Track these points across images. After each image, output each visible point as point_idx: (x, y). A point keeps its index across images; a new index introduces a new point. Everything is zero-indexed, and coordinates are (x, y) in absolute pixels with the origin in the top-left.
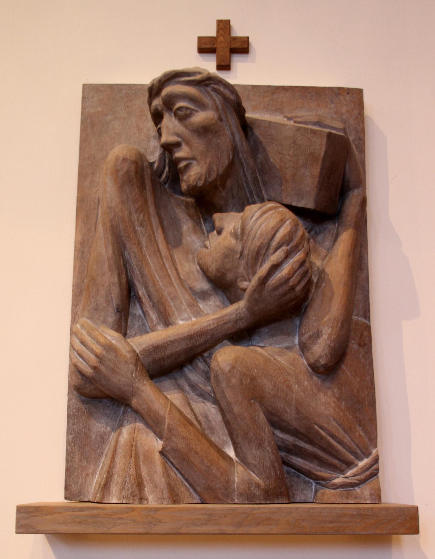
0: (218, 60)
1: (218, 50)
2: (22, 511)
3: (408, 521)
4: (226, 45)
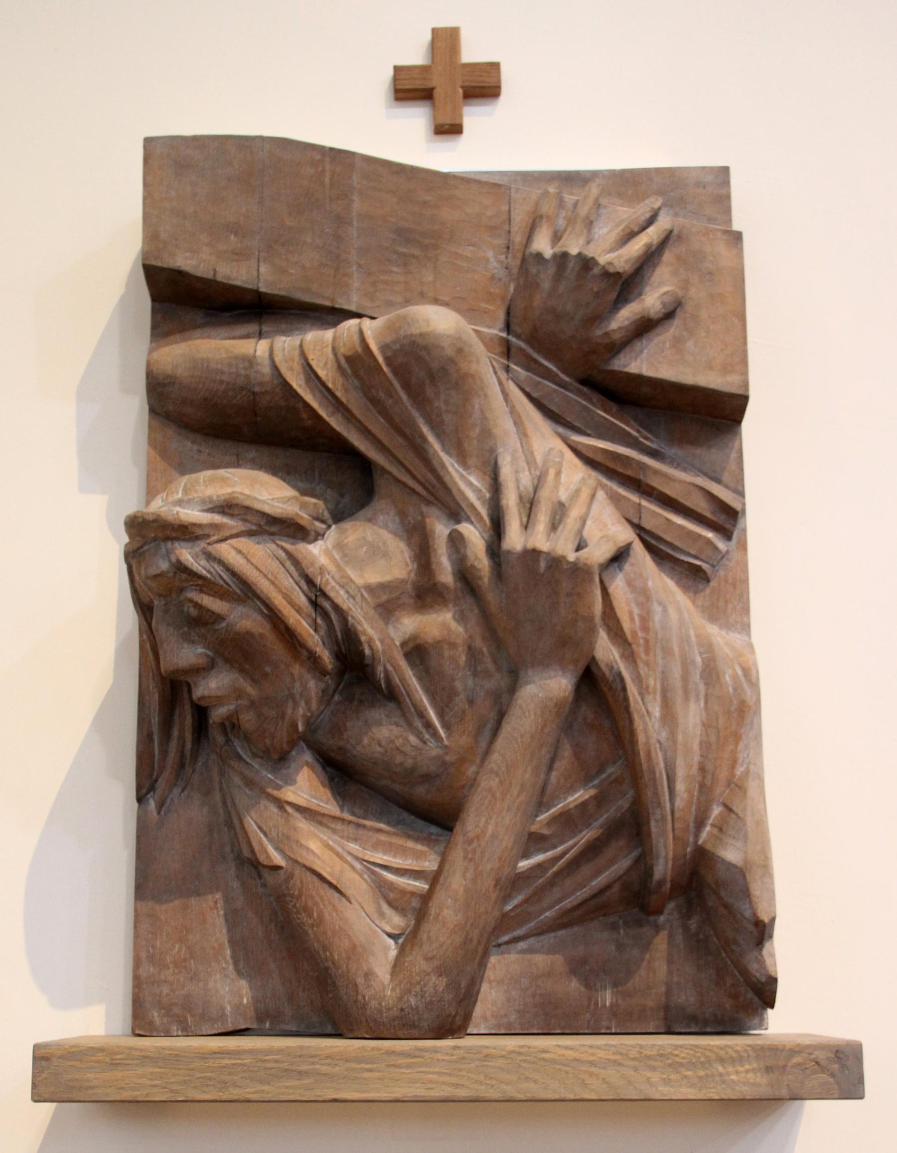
2: (44, 1058)
3: (838, 1071)
4: (445, 85)
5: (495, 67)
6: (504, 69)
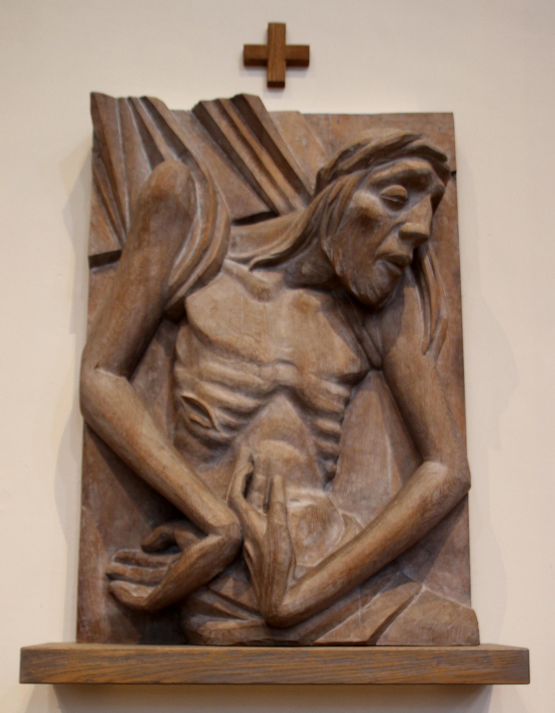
1: (270, 64)
2: (523, 677)
3: (514, 666)
4: (278, 57)
5: (306, 49)
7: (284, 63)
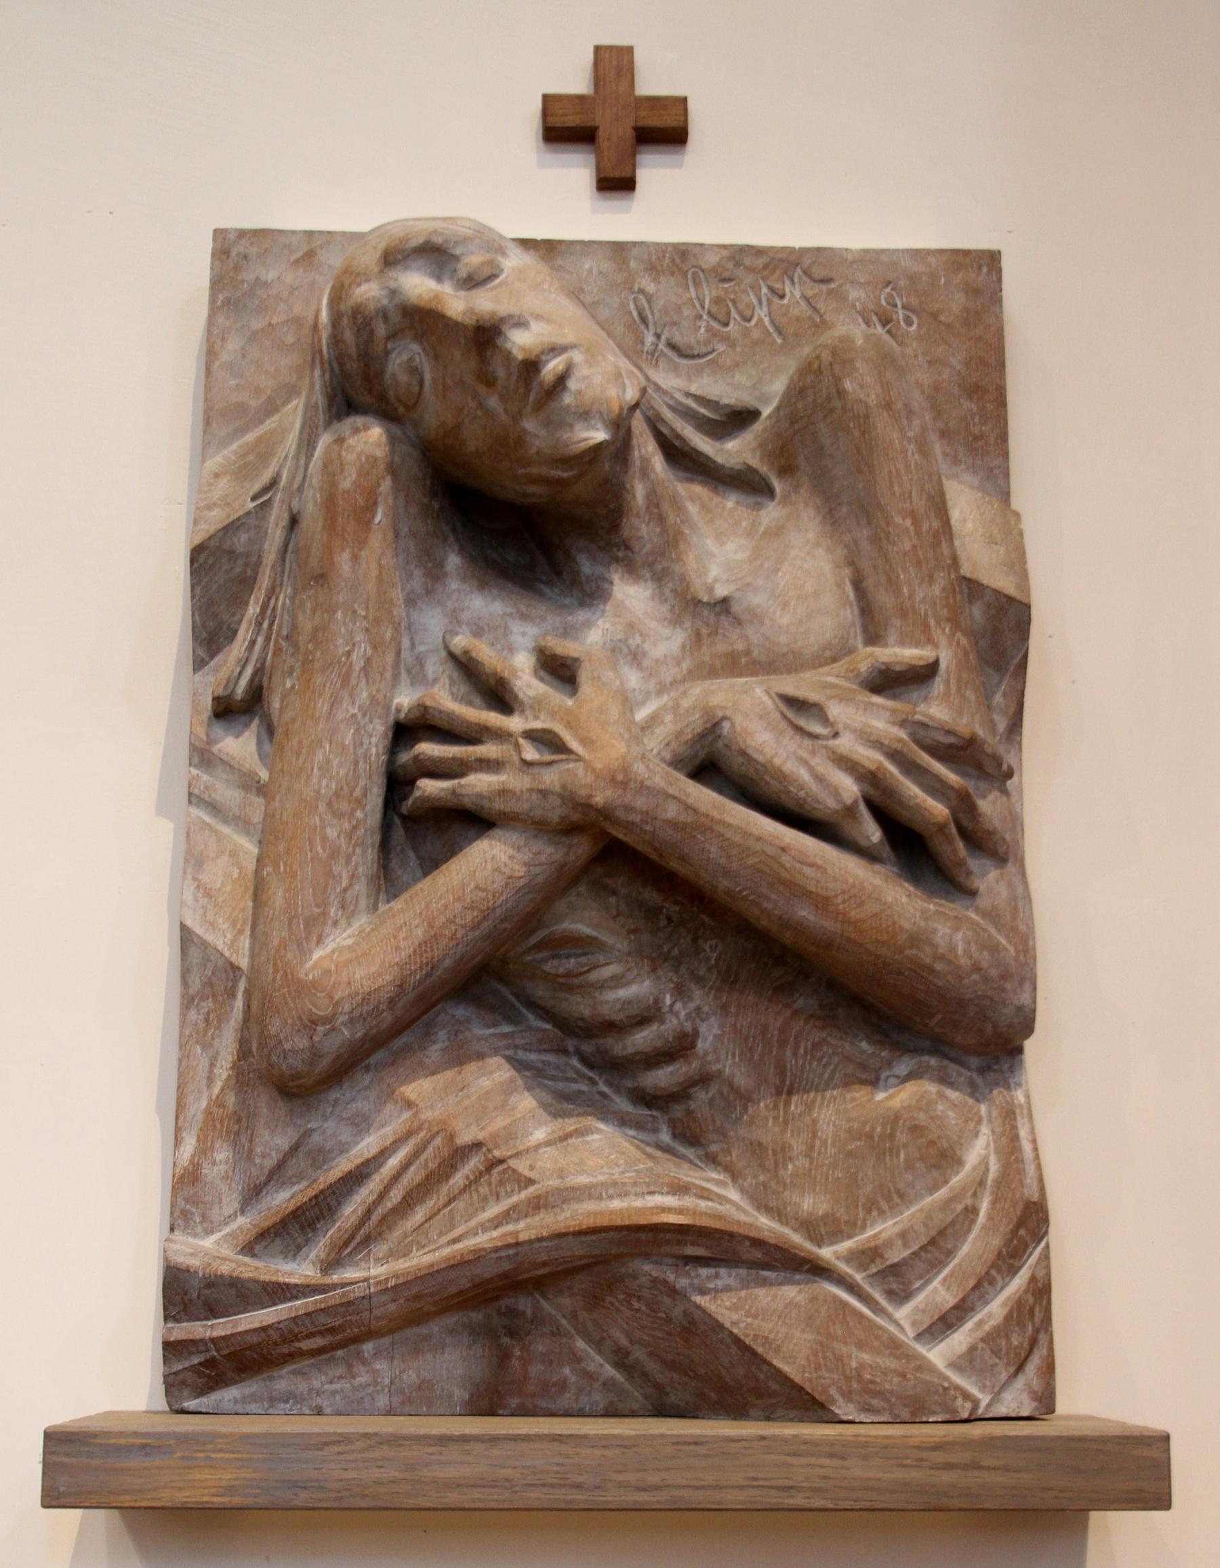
0: (599, 169)
2: (62, 1445)
3: (1136, 1471)
6: (692, 106)
7: (629, 134)
